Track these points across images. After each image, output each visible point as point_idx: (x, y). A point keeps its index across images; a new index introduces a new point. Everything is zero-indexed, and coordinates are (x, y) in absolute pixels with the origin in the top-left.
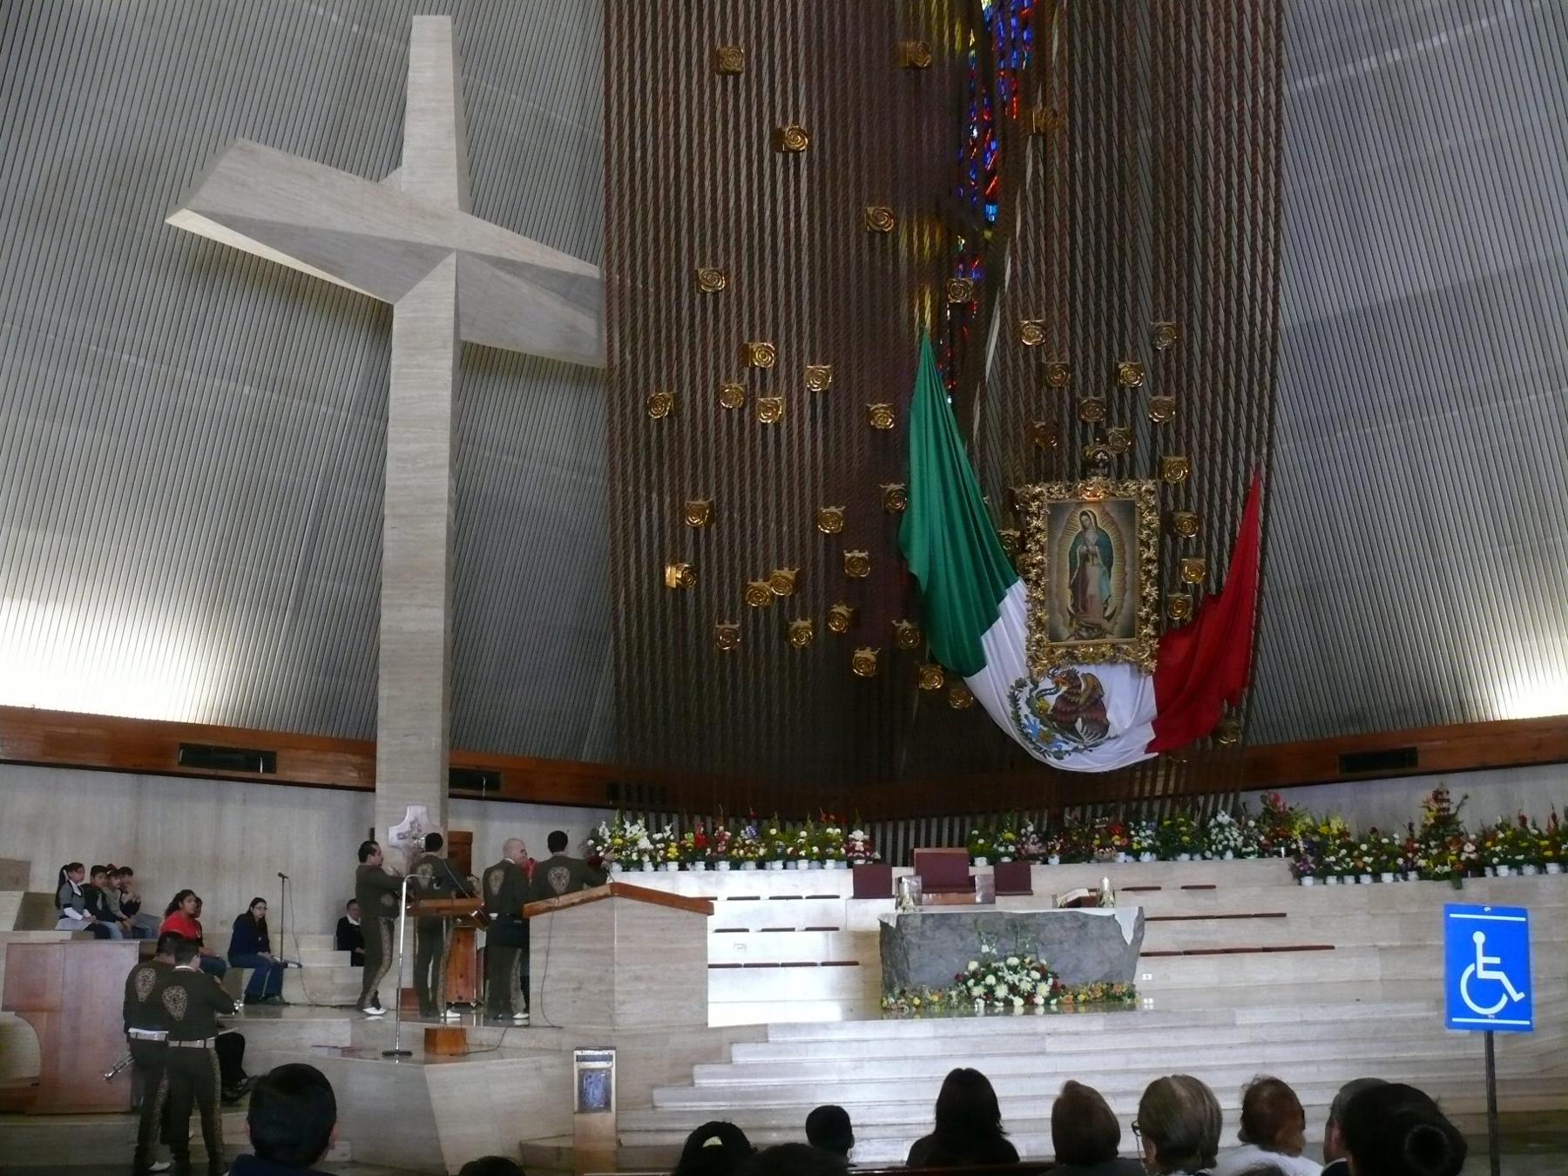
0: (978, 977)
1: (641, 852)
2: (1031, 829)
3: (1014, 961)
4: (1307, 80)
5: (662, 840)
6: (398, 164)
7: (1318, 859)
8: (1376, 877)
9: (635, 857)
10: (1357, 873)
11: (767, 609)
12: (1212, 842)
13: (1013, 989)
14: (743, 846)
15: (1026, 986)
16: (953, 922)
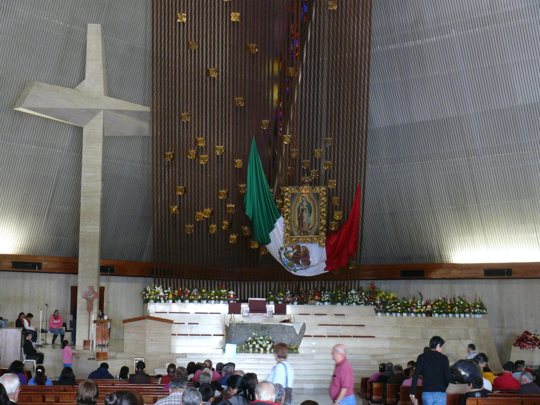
0: (251, 342)
1: (160, 296)
2: (289, 292)
3: (261, 338)
4: (392, 46)
5: (167, 293)
6: (84, 79)
7: (385, 307)
8: (401, 313)
9: (158, 298)
10: (396, 312)
11: (203, 221)
12: (348, 300)
13: (261, 346)
14: (194, 295)
15: (264, 345)
16: (245, 326)
